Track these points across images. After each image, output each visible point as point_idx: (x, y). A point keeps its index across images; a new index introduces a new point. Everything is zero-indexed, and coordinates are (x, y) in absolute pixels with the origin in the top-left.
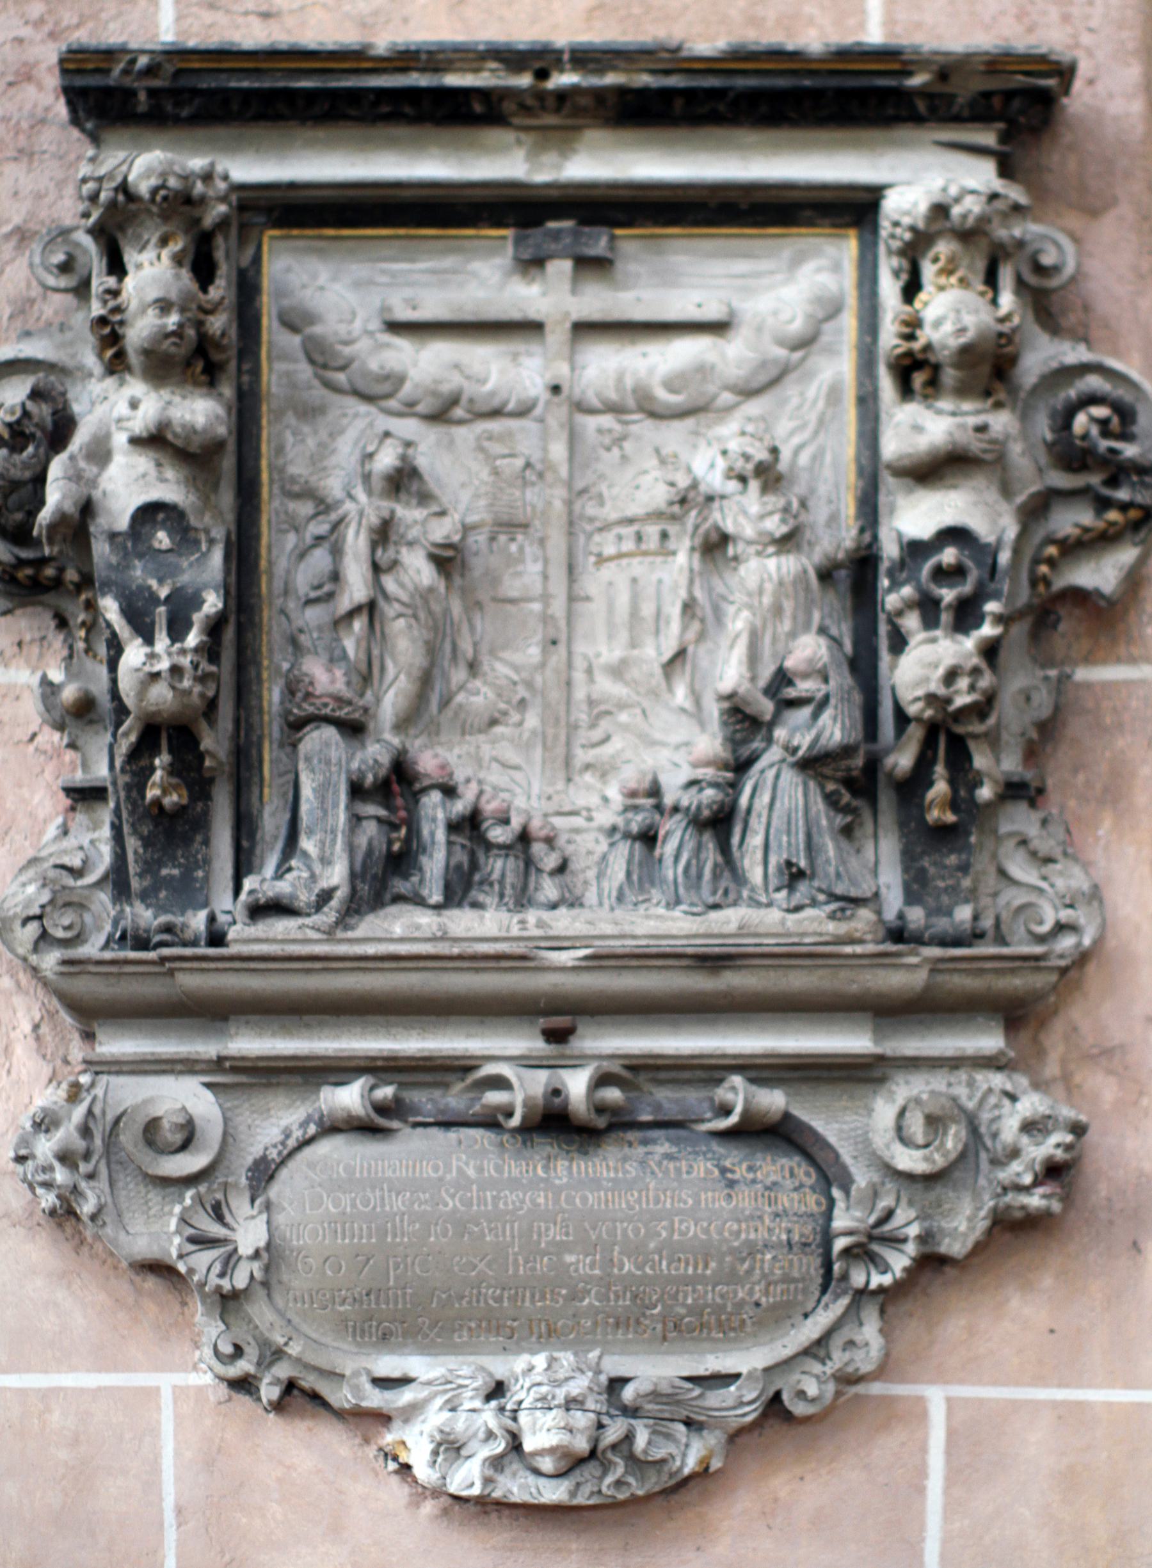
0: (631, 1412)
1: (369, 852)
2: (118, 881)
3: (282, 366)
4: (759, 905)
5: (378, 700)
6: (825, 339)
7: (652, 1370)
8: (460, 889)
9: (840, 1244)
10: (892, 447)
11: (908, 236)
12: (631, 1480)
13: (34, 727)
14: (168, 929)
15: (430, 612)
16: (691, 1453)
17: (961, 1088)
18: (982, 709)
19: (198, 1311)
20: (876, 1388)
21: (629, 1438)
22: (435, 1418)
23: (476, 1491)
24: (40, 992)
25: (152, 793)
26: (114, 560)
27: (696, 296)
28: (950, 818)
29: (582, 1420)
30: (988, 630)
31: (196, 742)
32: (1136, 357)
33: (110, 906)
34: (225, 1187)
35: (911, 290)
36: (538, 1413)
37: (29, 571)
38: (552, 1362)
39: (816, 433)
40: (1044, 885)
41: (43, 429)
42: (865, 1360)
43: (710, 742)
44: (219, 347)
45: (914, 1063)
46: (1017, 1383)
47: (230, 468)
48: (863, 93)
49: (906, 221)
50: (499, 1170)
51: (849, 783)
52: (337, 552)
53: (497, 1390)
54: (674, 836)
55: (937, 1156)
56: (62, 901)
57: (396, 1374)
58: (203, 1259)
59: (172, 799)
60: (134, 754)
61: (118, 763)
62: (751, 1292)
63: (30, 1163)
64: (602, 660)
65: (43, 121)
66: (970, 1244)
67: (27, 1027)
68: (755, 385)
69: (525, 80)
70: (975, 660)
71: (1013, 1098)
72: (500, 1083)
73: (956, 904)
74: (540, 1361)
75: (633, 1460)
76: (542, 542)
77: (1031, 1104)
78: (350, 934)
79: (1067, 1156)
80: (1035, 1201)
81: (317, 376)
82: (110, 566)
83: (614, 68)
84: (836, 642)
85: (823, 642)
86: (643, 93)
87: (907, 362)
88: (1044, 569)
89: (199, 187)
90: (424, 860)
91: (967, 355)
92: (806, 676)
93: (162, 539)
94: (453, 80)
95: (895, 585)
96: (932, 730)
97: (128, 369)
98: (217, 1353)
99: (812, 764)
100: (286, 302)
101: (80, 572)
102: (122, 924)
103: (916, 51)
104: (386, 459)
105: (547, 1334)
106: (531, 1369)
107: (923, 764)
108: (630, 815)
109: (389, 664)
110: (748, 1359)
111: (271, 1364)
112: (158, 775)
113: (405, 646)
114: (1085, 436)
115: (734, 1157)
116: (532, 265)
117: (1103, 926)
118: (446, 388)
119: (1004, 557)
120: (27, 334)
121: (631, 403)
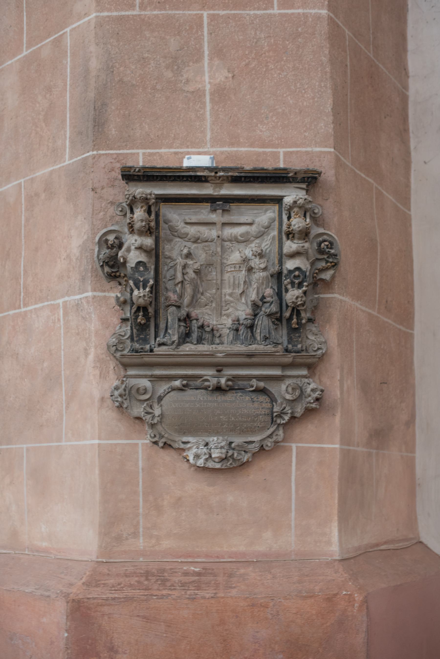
0: (234, 449)
1: (182, 333)
2: (132, 338)
3: (164, 232)
4: (259, 344)
5: (183, 301)
6: (272, 227)
7: (238, 440)
8: (200, 341)
9: (275, 414)
10: (286, 250)
11: (289, 207)
12: (233, 463)
13: (114, 305)
14: (142, 349)
15: (194, 283)
16: (246, 458)
17: (298, 381)
18: (303, 305)
19: (147, 428)
20: (282, 444)
21: (233, 454)
22: (194, 450)
23: (202, 465)
24: (115, 360)
25: (139, 320)
26: (132, 273)
27: (246, 218)
28: (297, 326)
29: (224, 451)
30: (304, 288)
31: (148, 310)
32: (333, 231)
33: (130, 343)
34: (153, 402)
35: (289, 218)
36: (215, 450)
37: (114, 274)
38: (218, 439)
39: (270, 247)
40: (315, 340)
41: (117, 245)
42: (280, 438)
43: (249, 310)
44: (152, 229)
45: (290, 377)
46: (310, 443)
47: (155, 253)
48: (279, 177)
49: (288, 204)
50: (207, 398)
51: (277, 319)
52: (175, 271)
53: (207, 444)
54: (242, 328)
55: (294, 396)
56: (121, 342)
57: (186, 441)
58: (148, 417)
59: (143, 322)
60: (135, 312)
61: (132, 314)
62: (257, 424)
63: (113, 397)
64: (228, 293)
65: (116, 179)
66: (301, 414)
67: (112, 368)
68: (258, 236)
69: (213, 174)
70: (302, 295)
71: (309, 384)
72: (207, 380)
73: (298, 344)
74: (215, 439)
75: (234, 460)
76: (216, 268)
77: (313, 386)
78: (178, 350)
79: (320, 396)
80: (314, 406)
81: (171, 233)
82: (131, 274)
83: (231, 172)
84: (274, 289)
85: (272, 290)
86: (236, 177)
87: (288, 233)
88: (315, 275)
89: (149, 197)
90: (193, 334)
91: (300, 232)
92: (268, 297)
93: (141, 269)
94: (199, 174)
95: (286, 279)
96: (293, 308)
97: (134, 233)
98: (151, 437)
99: (269, 315)
100: (165, 218)
101: (124, 274)
102: (133, 347)
103: (290, 169)
104: (185, 251)
105: (217, 433)
106: (213, 440)
107: (291, 315)
108: (233, 325)
109: (186, 293)
110: (257, 438)
111: (161, 439)
112: (140, 317)
113: (189, 290)
114: (323, 248)
115: (254, 396)
116: (214, 210)
117: (327, 349)
118: (197, 236)
119: (308, 274)
120: (112, 225)
121: (233, 240)
